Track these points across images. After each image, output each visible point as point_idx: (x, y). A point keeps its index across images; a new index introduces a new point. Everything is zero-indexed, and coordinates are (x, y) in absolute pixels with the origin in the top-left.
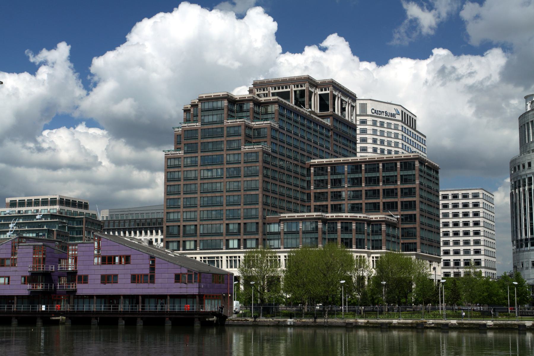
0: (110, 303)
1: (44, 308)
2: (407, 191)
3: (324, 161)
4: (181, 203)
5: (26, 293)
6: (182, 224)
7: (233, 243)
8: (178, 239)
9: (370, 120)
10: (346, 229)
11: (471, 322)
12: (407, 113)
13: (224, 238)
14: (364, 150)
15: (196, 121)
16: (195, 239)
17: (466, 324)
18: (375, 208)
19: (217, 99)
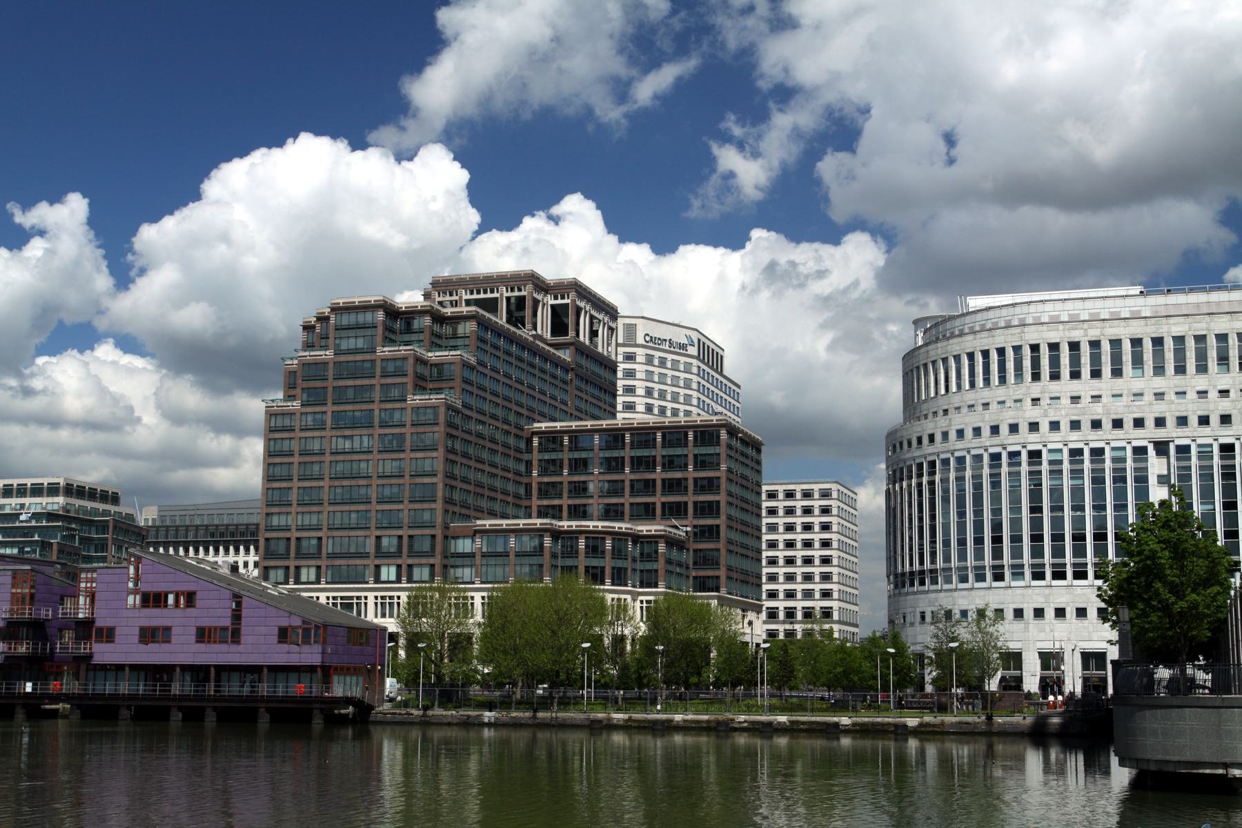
3: (558, 425)
7: (389, 573)
8: (286, 563)
10: (595, 549)
12: (707, 343)
14: (630, 407)
15: (326, 348)
16: (318, 563)
17: (803, 723)
18: (647, 512)
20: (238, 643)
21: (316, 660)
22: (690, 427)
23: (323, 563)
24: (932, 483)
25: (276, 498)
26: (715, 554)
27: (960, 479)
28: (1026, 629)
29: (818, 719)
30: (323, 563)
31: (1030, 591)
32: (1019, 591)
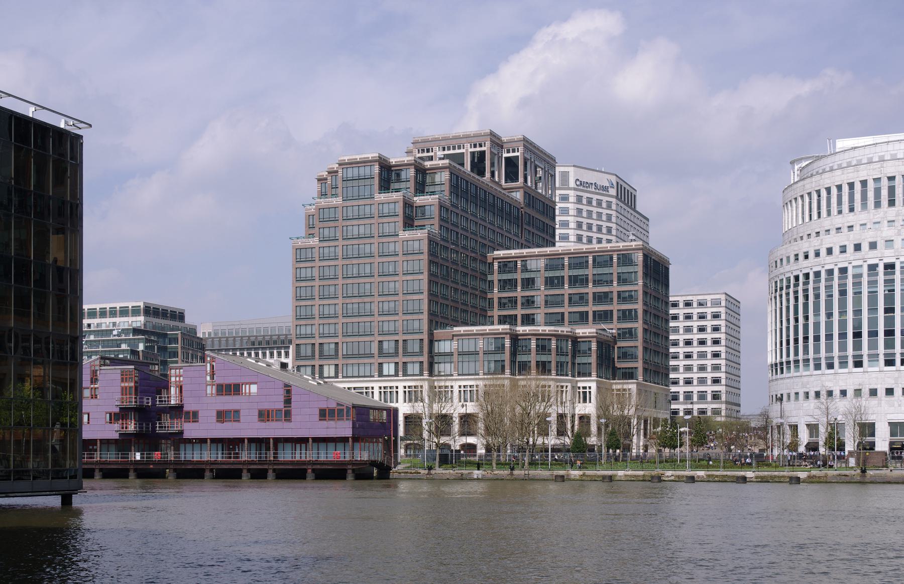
0: (229, 449)
1: (138, 457)
2: (577, 297)
3: (513, 252)
4: (316, 311)
5: (116, 436)
6: (318, 341)
7: (389, 369)
8: (313, 363)
9: (572, 194)
10: (543, 348)
11: (725, 473)
12: (624, 185)
13: (376, 360)
14: (565, 238)
15: (336, 195)
16: (336, 362)
17: (717, 476)
18: (583, 318)
19: (365, 162)
20: (290, 421)
21: (348, 433)
22: (614, 251)
23: (340, 362)
24: (806, 290)
25: (303, 313)
26: (633, 349)
27: (829, 287)
28: (879, 405)
29: (729, 473)
30: (340, 362)
31: (882, 374)
32: (874, 375)
